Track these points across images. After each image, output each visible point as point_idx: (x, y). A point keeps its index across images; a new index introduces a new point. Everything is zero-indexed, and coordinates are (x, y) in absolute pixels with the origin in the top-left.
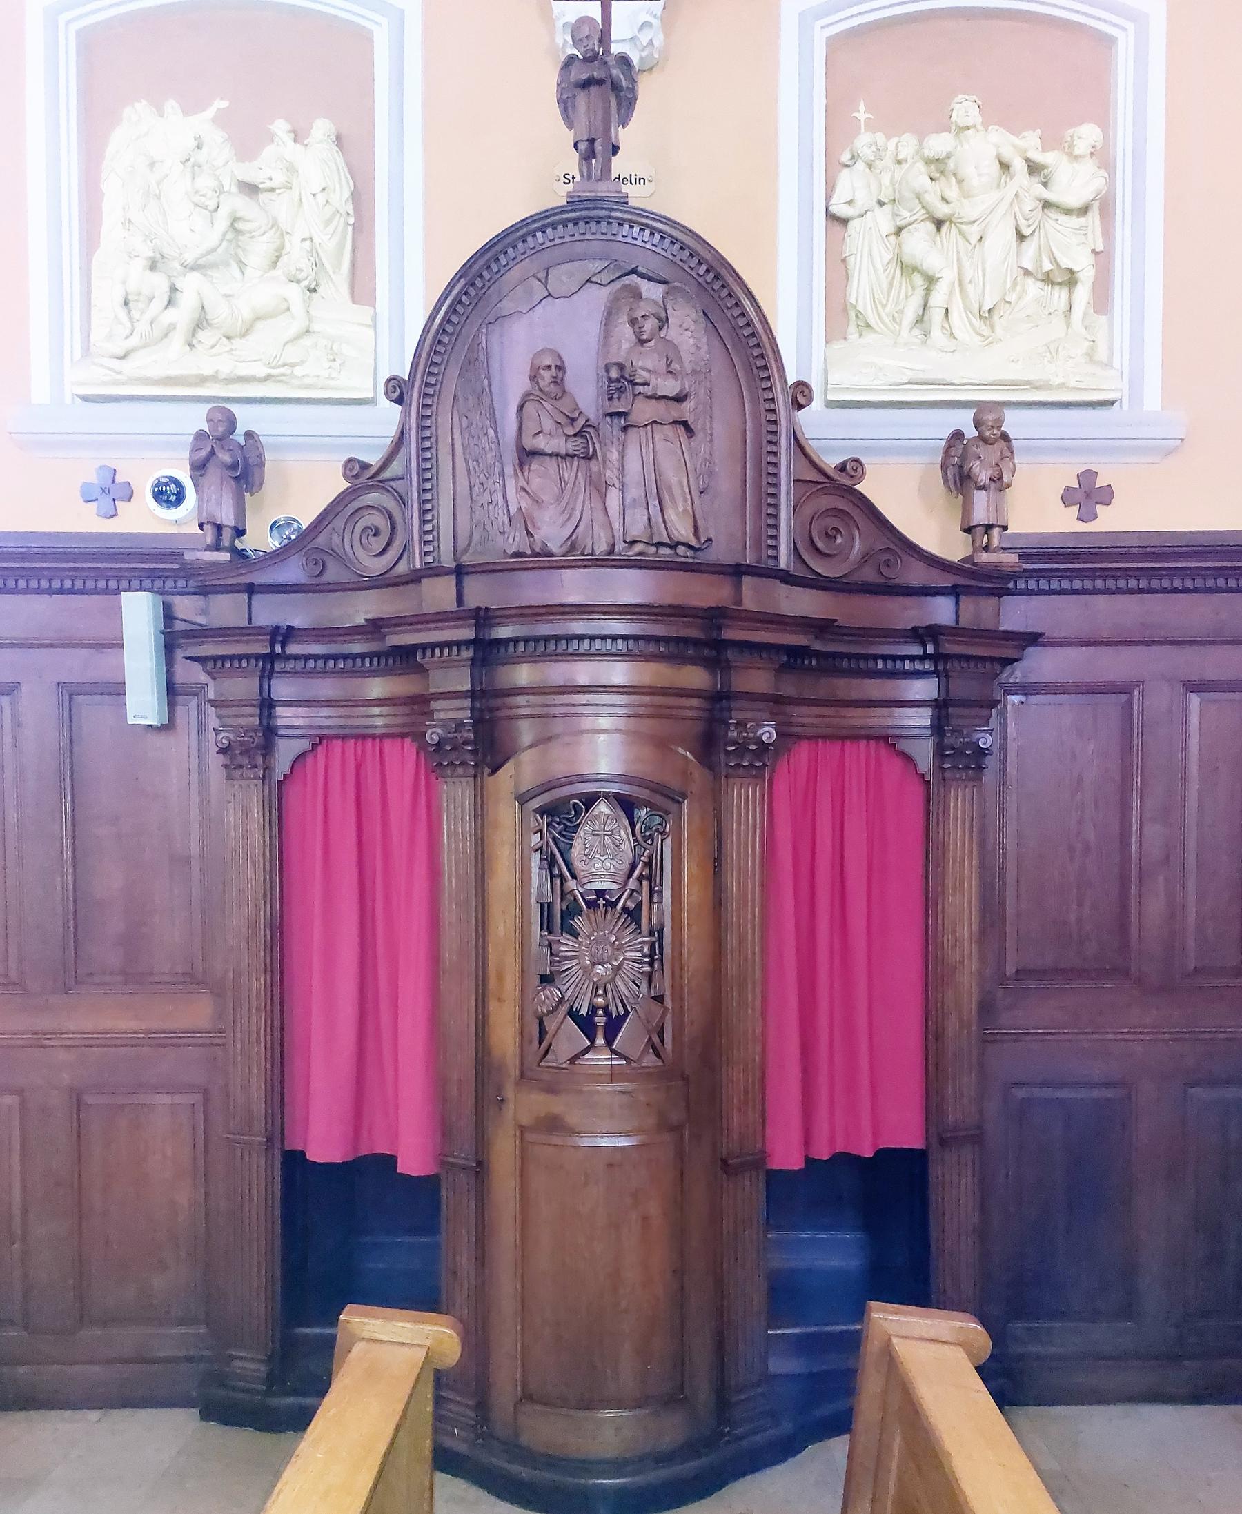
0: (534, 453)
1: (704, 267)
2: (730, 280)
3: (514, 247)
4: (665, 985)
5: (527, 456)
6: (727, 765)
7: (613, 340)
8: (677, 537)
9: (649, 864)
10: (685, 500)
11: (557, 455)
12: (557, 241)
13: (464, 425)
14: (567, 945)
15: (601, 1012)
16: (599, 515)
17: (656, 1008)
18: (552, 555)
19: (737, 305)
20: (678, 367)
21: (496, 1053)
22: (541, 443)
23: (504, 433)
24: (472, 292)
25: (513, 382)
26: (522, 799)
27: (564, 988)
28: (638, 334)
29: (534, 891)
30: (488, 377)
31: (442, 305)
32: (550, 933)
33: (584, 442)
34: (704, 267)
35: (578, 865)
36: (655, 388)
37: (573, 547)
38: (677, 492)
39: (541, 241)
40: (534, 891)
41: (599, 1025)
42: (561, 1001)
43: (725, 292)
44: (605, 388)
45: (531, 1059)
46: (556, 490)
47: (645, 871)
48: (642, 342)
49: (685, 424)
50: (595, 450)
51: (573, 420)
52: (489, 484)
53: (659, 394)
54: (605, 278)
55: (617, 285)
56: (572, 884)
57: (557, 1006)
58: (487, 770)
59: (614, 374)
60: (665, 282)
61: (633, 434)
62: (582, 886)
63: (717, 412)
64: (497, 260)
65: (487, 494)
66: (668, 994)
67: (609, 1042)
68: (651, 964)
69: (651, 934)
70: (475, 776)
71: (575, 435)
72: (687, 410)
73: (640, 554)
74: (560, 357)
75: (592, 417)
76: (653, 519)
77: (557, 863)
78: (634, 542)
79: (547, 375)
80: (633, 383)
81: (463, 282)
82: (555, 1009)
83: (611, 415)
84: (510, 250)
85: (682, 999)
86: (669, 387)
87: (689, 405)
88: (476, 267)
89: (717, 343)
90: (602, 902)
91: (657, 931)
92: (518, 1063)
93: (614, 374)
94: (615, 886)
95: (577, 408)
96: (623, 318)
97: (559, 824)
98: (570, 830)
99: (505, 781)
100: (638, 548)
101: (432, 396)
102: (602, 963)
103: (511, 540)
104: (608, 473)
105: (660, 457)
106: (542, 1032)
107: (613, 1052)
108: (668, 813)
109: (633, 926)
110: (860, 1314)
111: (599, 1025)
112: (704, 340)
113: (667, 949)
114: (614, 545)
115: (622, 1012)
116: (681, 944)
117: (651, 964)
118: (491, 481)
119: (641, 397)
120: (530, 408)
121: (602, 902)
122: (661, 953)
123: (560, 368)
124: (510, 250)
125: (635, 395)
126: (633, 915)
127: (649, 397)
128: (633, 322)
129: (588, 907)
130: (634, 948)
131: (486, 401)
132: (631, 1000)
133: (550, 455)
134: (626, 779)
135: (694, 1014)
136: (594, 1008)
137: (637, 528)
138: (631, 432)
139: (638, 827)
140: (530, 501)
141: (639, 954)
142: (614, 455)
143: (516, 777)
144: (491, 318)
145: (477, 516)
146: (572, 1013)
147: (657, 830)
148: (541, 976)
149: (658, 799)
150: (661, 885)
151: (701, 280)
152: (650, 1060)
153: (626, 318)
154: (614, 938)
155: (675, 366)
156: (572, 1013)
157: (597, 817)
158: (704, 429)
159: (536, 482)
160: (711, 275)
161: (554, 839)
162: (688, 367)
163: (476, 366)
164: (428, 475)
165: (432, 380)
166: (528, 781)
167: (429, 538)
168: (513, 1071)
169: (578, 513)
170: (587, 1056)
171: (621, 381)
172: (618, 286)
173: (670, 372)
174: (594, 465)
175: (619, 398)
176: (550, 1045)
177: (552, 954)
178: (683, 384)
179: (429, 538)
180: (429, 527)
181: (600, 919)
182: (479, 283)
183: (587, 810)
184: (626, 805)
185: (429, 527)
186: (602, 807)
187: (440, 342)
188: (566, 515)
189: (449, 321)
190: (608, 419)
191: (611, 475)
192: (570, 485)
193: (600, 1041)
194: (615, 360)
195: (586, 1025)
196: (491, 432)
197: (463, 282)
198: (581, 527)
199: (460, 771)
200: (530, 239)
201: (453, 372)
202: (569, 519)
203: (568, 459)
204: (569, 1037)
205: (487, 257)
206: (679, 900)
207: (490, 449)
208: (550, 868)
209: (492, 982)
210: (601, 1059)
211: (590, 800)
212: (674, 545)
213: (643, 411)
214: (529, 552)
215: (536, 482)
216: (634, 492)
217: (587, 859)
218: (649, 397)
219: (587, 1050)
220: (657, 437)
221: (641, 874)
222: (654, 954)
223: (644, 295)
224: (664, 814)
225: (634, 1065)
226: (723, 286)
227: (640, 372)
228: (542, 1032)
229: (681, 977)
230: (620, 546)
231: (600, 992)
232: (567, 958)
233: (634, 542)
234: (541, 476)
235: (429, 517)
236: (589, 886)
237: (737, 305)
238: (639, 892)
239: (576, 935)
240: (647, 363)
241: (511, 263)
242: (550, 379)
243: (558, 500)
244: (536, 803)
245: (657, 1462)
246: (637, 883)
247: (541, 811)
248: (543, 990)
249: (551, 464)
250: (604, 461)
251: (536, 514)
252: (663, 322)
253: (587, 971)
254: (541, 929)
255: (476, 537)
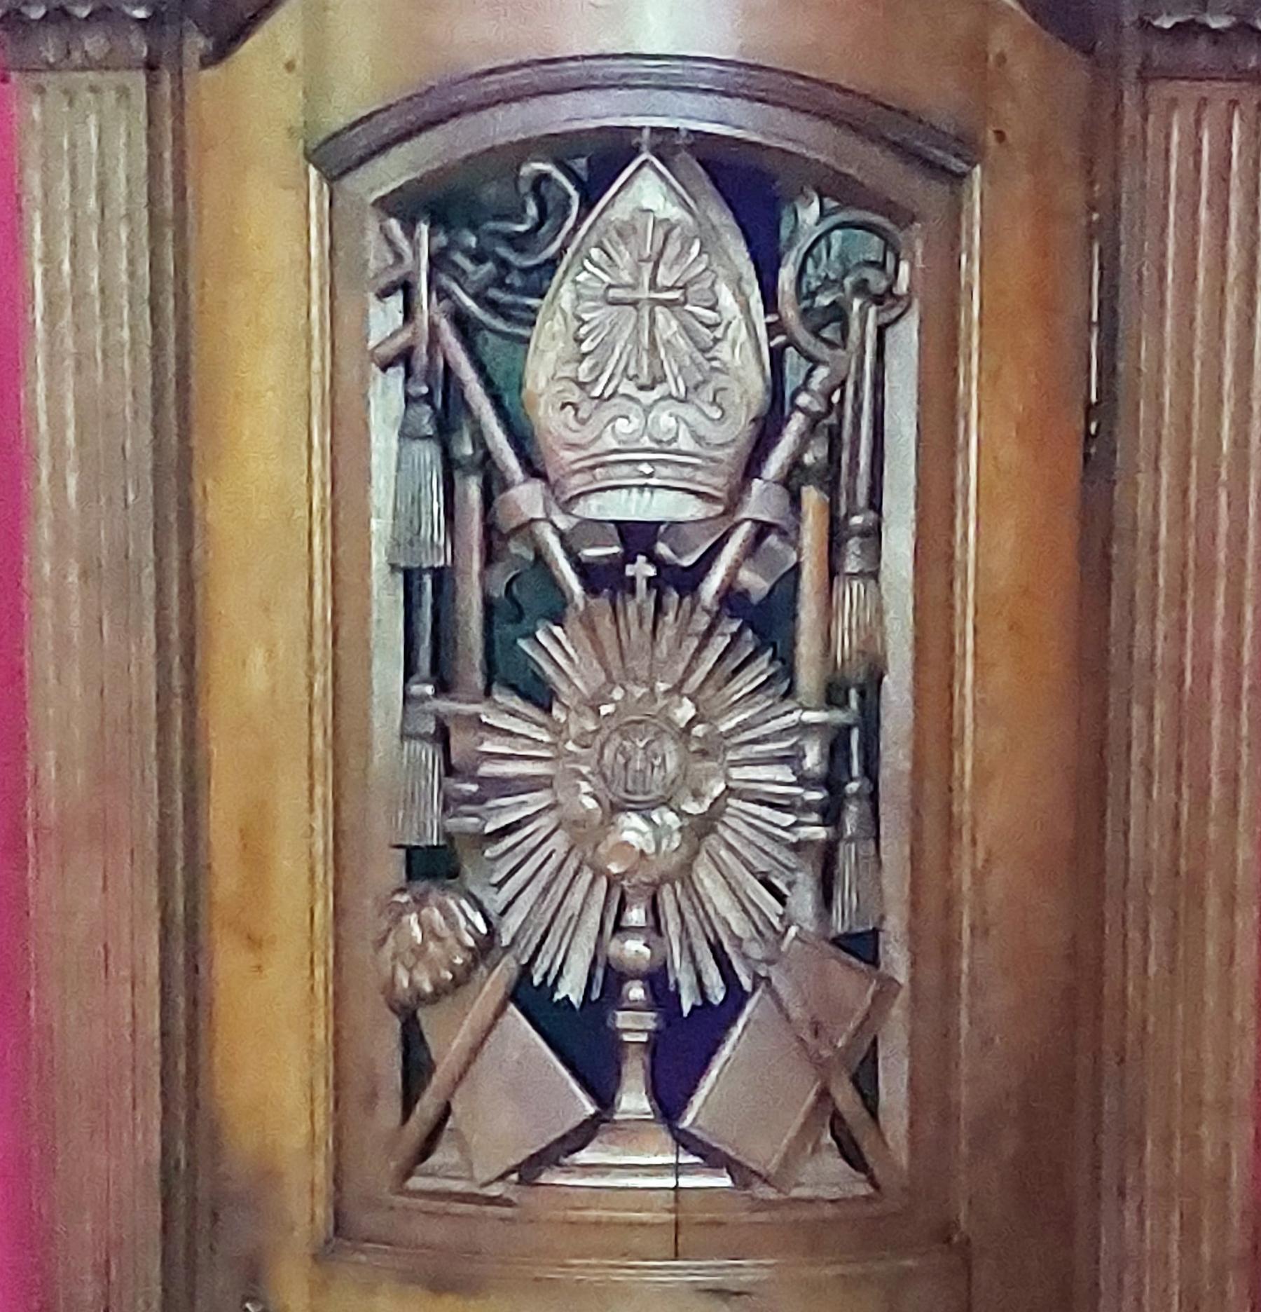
4: (885, 890)
6: (1145, 25)
9: (828, 426)
14: (509, 736)
15: (636, 992)
17: (847, 983)
21: (243, 1140)
26: (336, 157)
27: (496, 901)
29: (380, 527)
32: (444, 687)
35: (550, 421)
40: (380, 527)
41: (634, 1038)
42: (486, 947)
45: (375, 1170)
47: (809, 447)
56: (526, 498)
57: (470, 968)
58: (197, 43)
62: (566, 507)
66: (895, 925)
67: (669, 1105)
68: (831, 814)
69: (833, 695)
70: (151, 66)
77: (466, 411)
82: (462, 979)
85: (949, 948)
90: (642, 569)
91: (854, 687)
92: (321, 1170)
94: (692, 509)
97: (478, 257)
98: (518, 286)
99: (262, 90)
102: (653, 806)
106: (416, 1066)
107: (684, 1141)
108: (904, 216)
109: (762, 668)
110: (777, 1173)
111: (634, 1038)
113: (896, 757)
115: (717, 994)
116: (950, 742)
117: (831, 814)
121: (642, 569)
122: (871, 770)
126: (764, 621)
129: (591, 588)
130: (764, 752)
132: (756, 951)
134: (746, 80)
135: (994, 1009)
136: (609, 978)
139: (786, 275)
141: (784, 773)
143: (313, 70)
146: (530, 997)
147: (861, 288)
148: (410, 851)
149: (871, 164)
150: (875, 504)
152: (826, 1174)
154: (686, 711)
156: (530, 997)
157: (625, 232)
161: (461, 321)
166: (359, 85)
168: (303, 1208)
170: (583, 1157)
176: (447, 1111)
177: (450, 770)
181: (637, 635)
183: (588, 203)
184: (747, 188)
186: (647, 193)
193: (634, 1100)
195: (581, 1039)
199: (94, 43)
204: (514, 1087)
206: (936, 570)
208: (444, 432)
209: (226, 879)
210: (635, 1165)
211: (603, 161)
217: (587, 397)
219: (584, 1134)
221: (796, 463)
222: (844, 774)
224: (887, 217)
225: (764, 1192)
228: (416, 1066)
229: (947, 869)
231: (636, 916)
232: (505, 786)
236: (593, 508)
238: (790, 535)
239: (539, 694)
244: (393, 172)
246: (779, 498)
247: (405, 206)
248: (420, 902)
253: (585, 835)
254: (410, 671)
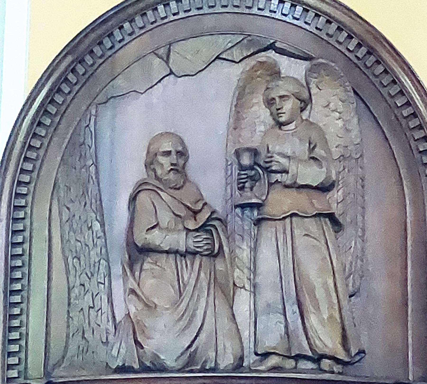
0: (147, 250)
1: (355, 42)
2: (385, 56)
3: (132, 21)
5: (138, 252)
7: (244, 123)
8: (321, 349)
10: (331, 306)
11: (176, 252)
12: (182, 15)
13: (65, 218)
16: (224, 322)
18: (164, 369)
19: (394, 82)
20: (323, 153)
22: (156, 238)
23: (112, 229)
24: (80, 69)
25: (125, 168)
28: (275, 115)
30: (96, 164)
31: (43, 85)
33: (210, 238)
34: (355, 42)
36: (295, 176)
37: (192, 360)
38: (320, 293)
39: (163, 15)
43: (380, 69)
44: (235, 176)
46: (172, 293)
48: (280, 125)
49: (331, 217)
50: (221, 247)
51: (195, 213)
52: (92, 286)
53: (300, 182)
54: (237, 54)
55: (252, 62)
59: (246, 160)
60: (307, 58)
61: (268, 231)
63: (370, 198)
64: (111, 35)
65: (88, 297)
71: (196, 230)
72: (334, 201)
73: (274, 369)
74: (182, 143)
75: (219, 209)
76: (291, 327)
78: (266, 355)
79: (165, 161)
80: (268, 171)
81: (69, 59)
83: (243, 206)
84: (127, 25)
86: (312, 175)
87: (337, 195)
88: (87, 42)
89: (368, 122)
93: (246, 160)
95: (201, 198)
96: (258, 99)
100: (273, 361)
101: (27, 184)
103: (115, 352)
104: (237, 273)
105: (301, 254)
112: (355, 120)
114: (242, 359)
118: (94, 281)
119: (277, 186)
120: (143, 197)
123: (182, 154)
124: (127, 25)
125: (270, 184)
127: (287, 187)
128: (270, 102)
131: (92, 188)
133: (167, 252)
137: (272, 339)
138: (265, 225)
140: (140, 306)
142: (244, 253)
144: (101, 98)
145: (75, 323)
151: (351, 56)
153: (261, 98)
155: (319, 152)
158: (354, 222)
159: (149, 284)
160: (363, 50)
162: (336, 153)
163: (81, 153)
164: (18, 275)
165: (29, 166)
167: (14, 348)
169: (200, 313)
171: (254, 170)
172: (253, 63)
173: (313, 158)
174: (220, 266)
175: (251, 189)
178: (329, 171)
179: (14, 348)
180: (15, 335)
182: (89, 60)
185: (15, 335)
187: (40, 124)
188: (186, 318)
189: (52, 101)
190: (238, 210)
191: (240, 275)
192: (190, 288)
194: (249, 145)
196: (97, 226)
197: (69, 59)
198: (203, 336)
200: (150, 13)
201: (55, 157)
202: (187, 327)
203: (189, 257)
205: (99, 32)
207: (95, 245)
212: (317, 359)
213: (281, 202)
214: (136, 366)
215: (149, 284)
216: (269, 295)
218: (287, 187)
220: (296, 232)
223: (284, 72)
226: (378, 62)
227: (277, 158)
230: (250, 359)
233: (266, 355)
234: (156, 279)
235: (16, 323)
237: (394, 82)
240: (286, 147)
241: (128, 39)
242: (170, 166)
243: (176, 304)
245: (261, 362)
249: (168, 263)
250: (232, 260)
251: (148, 322)
252: (305, 103)
255: (72, 349)
